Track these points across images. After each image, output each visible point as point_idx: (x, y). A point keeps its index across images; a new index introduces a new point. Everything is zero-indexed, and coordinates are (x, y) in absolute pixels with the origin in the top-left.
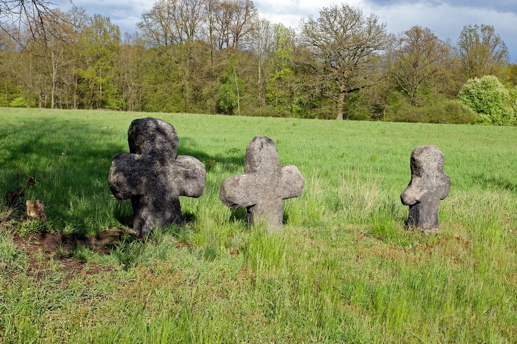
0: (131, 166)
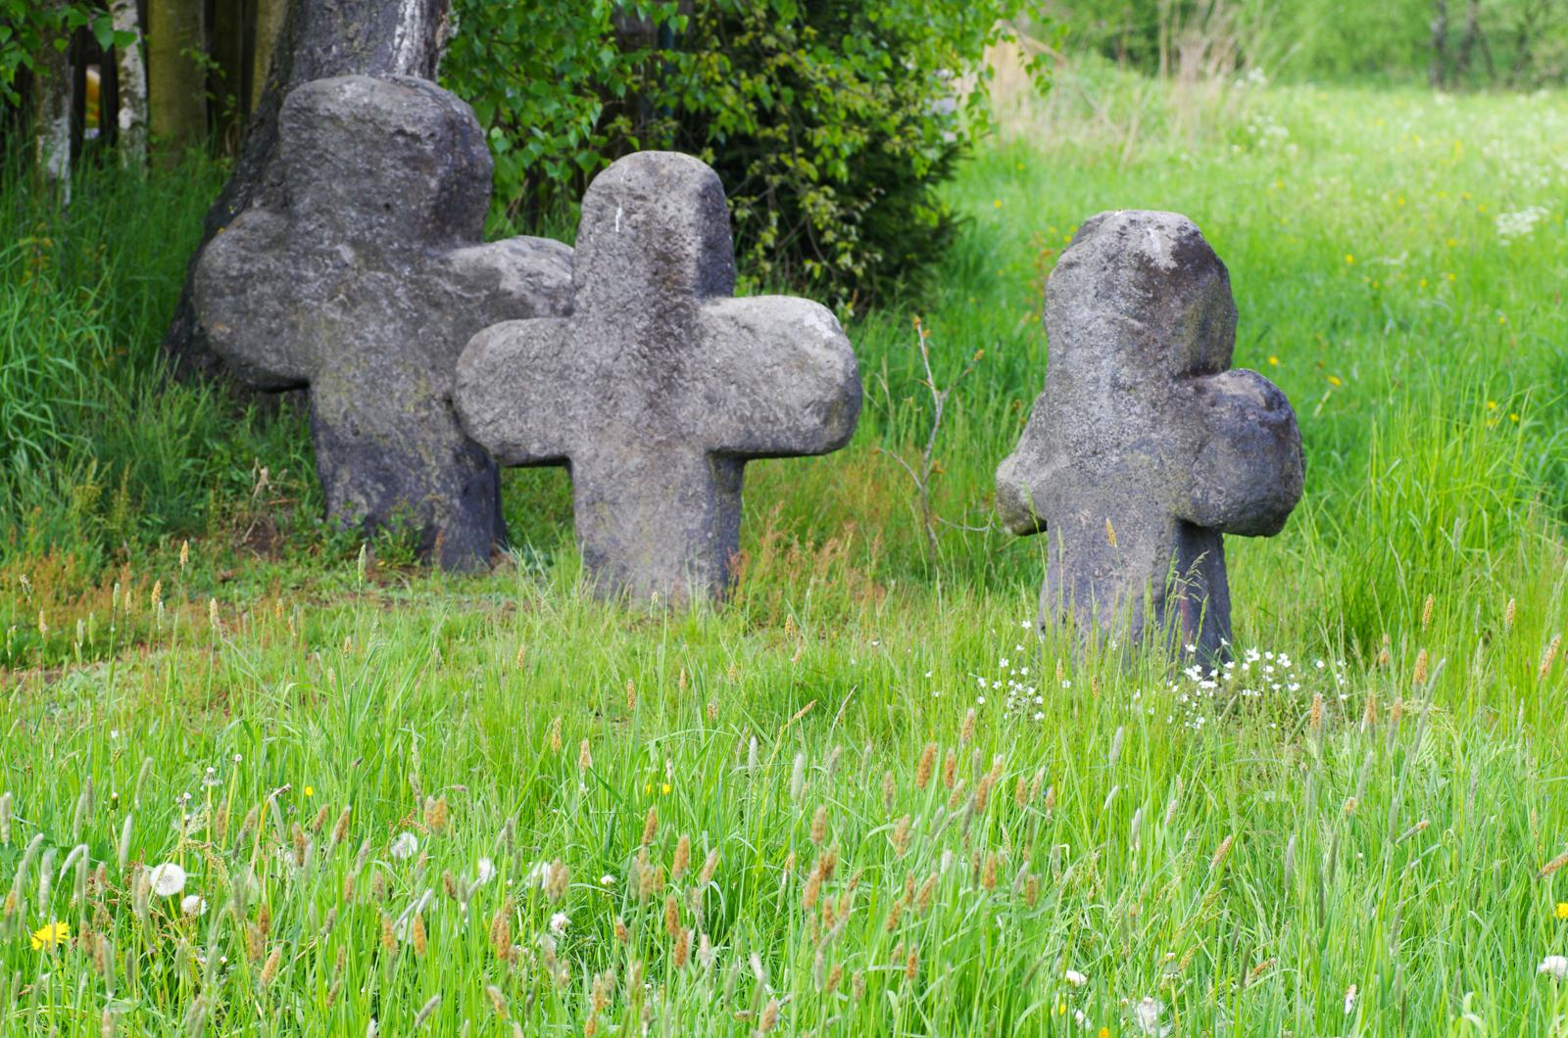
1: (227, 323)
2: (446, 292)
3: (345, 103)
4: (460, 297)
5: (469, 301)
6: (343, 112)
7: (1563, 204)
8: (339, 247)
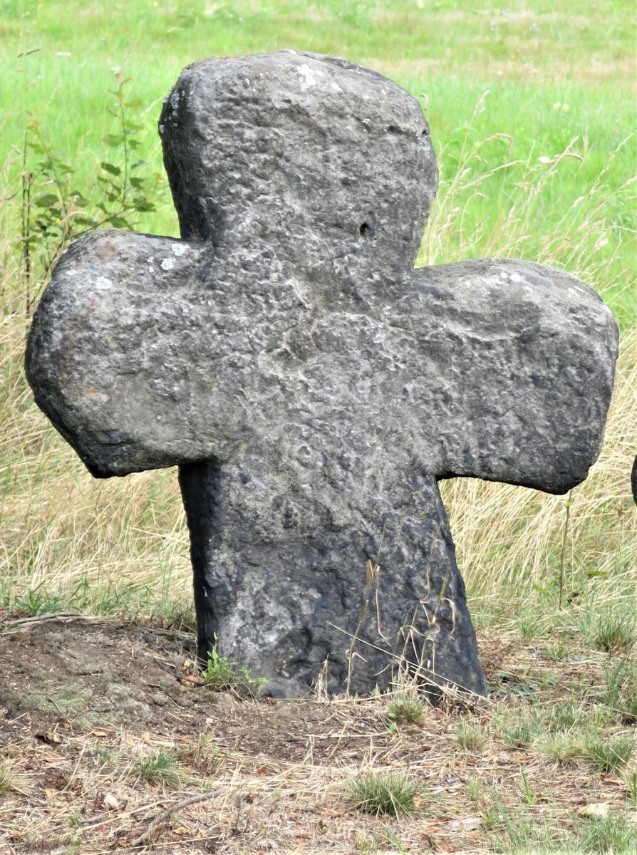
0: (138, 303)
1: (106, 388)
2: (451, 336)
3: (311, 92)
4: (474, 341)
5: (489, 346)
6: (308, 102)
7: (635, 444)
8: (288, 283)
